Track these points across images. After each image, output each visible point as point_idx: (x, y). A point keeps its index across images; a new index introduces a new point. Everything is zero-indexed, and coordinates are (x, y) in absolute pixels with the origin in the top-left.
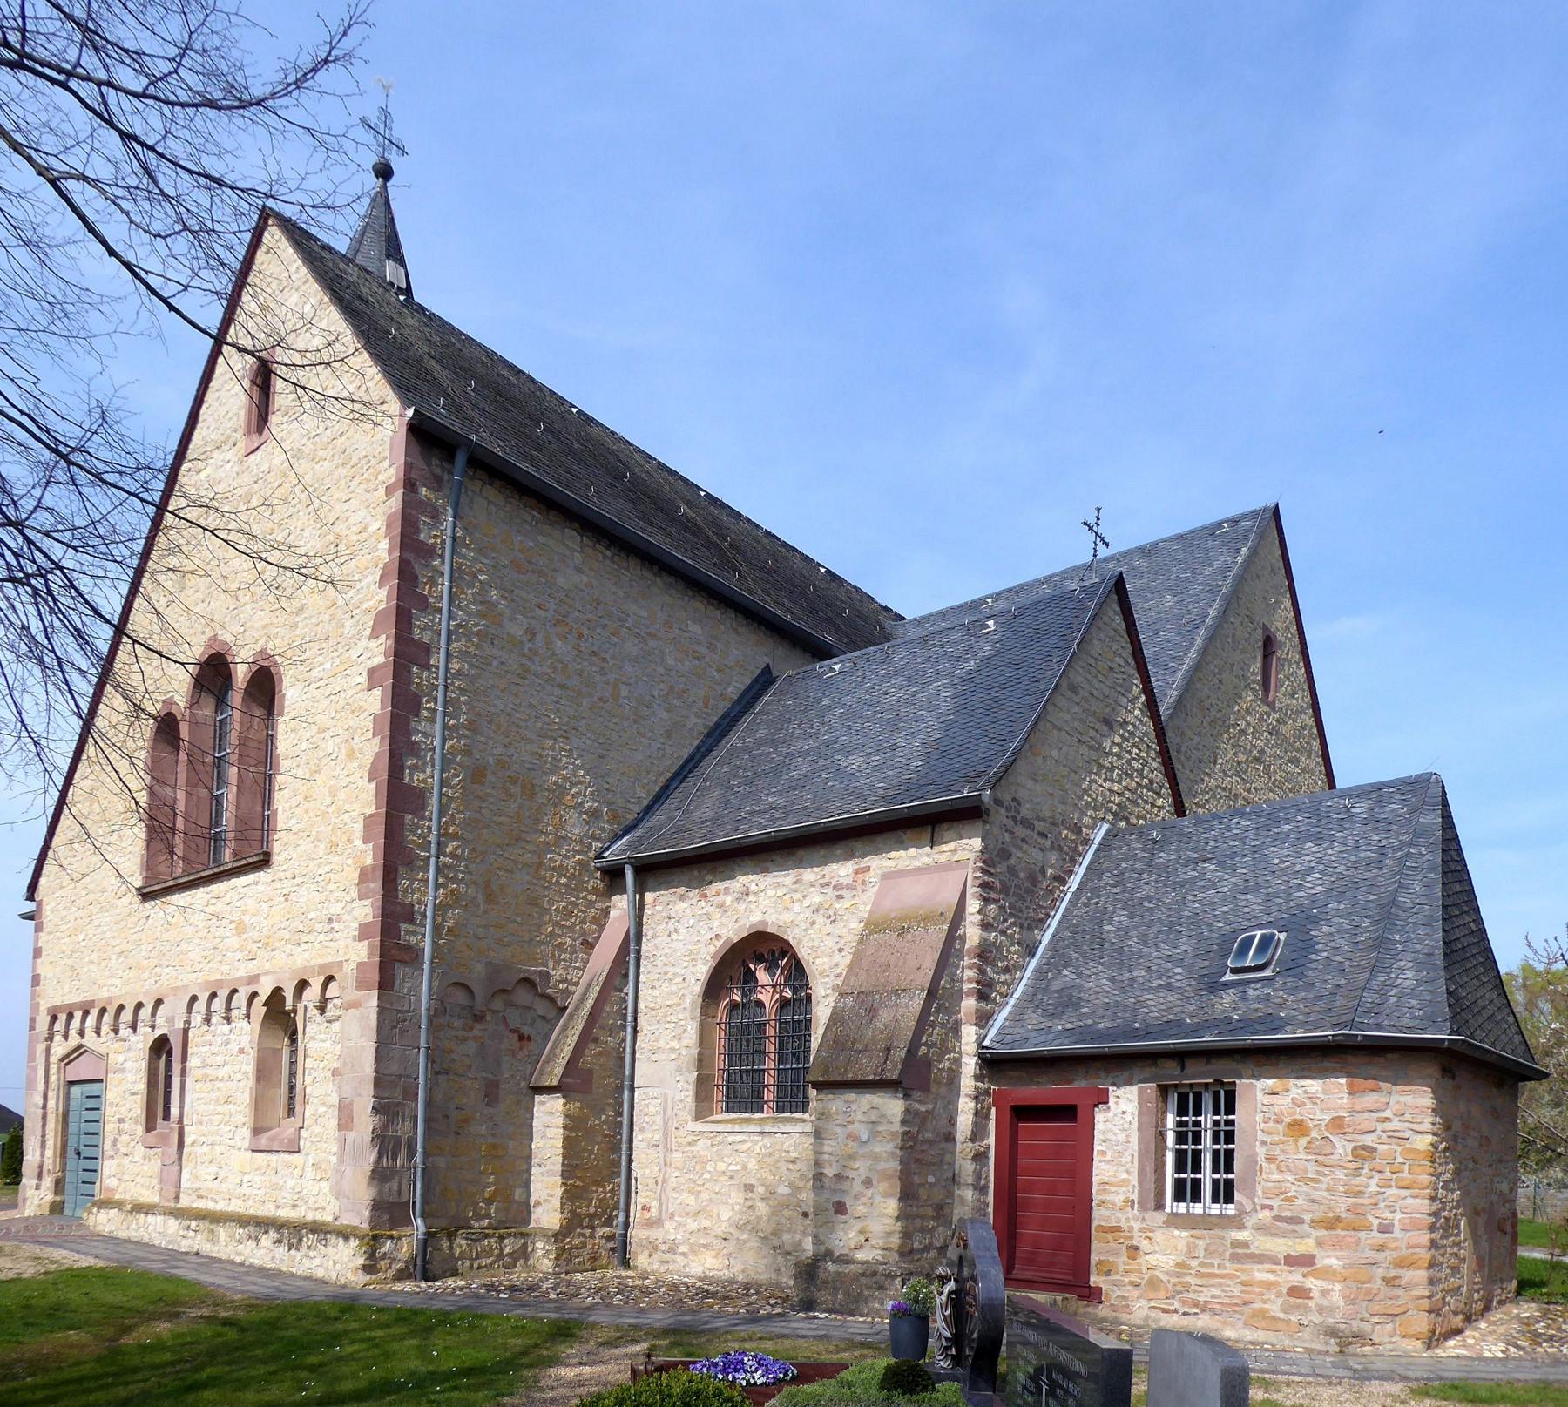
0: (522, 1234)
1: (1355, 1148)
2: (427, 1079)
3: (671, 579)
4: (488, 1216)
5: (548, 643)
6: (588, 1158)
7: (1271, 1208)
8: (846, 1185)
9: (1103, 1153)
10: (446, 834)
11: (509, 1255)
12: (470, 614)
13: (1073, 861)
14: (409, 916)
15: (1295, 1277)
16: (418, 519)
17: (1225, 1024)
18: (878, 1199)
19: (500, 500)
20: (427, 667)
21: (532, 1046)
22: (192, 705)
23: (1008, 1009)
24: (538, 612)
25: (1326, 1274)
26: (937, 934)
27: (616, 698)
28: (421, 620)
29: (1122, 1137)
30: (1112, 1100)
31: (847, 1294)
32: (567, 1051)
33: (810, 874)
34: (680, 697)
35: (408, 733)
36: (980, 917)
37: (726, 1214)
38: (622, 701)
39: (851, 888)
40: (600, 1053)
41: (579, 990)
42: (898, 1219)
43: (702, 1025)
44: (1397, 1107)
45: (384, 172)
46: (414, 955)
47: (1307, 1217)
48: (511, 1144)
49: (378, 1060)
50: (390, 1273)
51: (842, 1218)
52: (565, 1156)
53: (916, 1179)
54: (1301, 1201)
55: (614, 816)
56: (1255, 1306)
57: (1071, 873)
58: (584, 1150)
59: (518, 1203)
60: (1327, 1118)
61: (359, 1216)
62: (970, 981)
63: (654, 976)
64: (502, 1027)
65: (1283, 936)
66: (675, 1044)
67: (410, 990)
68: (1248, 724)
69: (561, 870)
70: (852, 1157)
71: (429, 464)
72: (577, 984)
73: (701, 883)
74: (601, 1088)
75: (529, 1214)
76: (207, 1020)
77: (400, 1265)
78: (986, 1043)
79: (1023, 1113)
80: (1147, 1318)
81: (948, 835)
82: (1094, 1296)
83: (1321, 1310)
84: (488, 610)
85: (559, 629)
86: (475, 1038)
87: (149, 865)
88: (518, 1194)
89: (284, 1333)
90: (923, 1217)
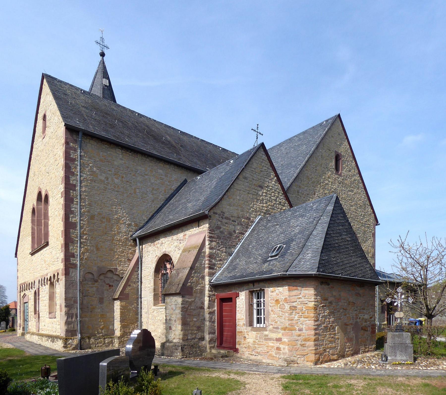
1: (290, 307)
2: (80, 298)
3: (152, 159)
4: (102, 333)
5: (113, 180)
6: (129, 317)
7: (272, 325)
8: (171, 322)
9: (238, 311)
10: (83, 234)
11: (107, 343)
12: (88, 175)
13: (247, 228)
14: (73, 256)
15: (277, 344)
16: (70, 152)
17: (263, 273)
18: (177, 325)
19: (95, 144)
20: (75, 190)
21: (113, 288)
22: (37, 205)
23: (221, 271)
24: (109, 172)
25: (284, 343)
26: (195, 252)
27: (135, 193)
28: (72, 178)
29: (242, 306)
30: (240, 296)
31: (170, 351)
33: (175, 237)
34: (156, 191)
35: (70, 208)
36: (209, 246)
37: (160, 331)
38: (137, 194)
39: (183, 240)
42: (182, 330)
43: (154, 280)
44: (303, 294)
45: (103, 55)
46: (75, 266)
47: (280, 327)
48: (108, 314)
49: (65, 294)
50: (71, 348)
51: (171, 331)
52: (121, 317)
53: (188, 320)
54: (278, 323)
55: (136, 225)
56: (270, 353)
57: (246, 231)
58: (127, 315)
60: (284, 298)
61: (63, 335)
62: (207, 264)
63: (145, 268)
65: (284, 246)
66: (149, 286)
67: (74, 275)
68: (329, 182)
69: (120, 241)
70: (172, 314)
71: (72, 137)
72: (126, 271)
73: (154, 242)
74: (131, 299)
75: (114, 332)
76: (42, 285)
77: (74, 346)
78: (212, 281)
79: (223, 300)
80: (247, 357)
81: (202, 224)
82: (236, 350)
83: (283, 353)
84: (93, 173)
85: (116, 176)
86: (96, 287)
87: (33, 247)
88: (111, 327)
89: (283, 375)
90: (192, 330)
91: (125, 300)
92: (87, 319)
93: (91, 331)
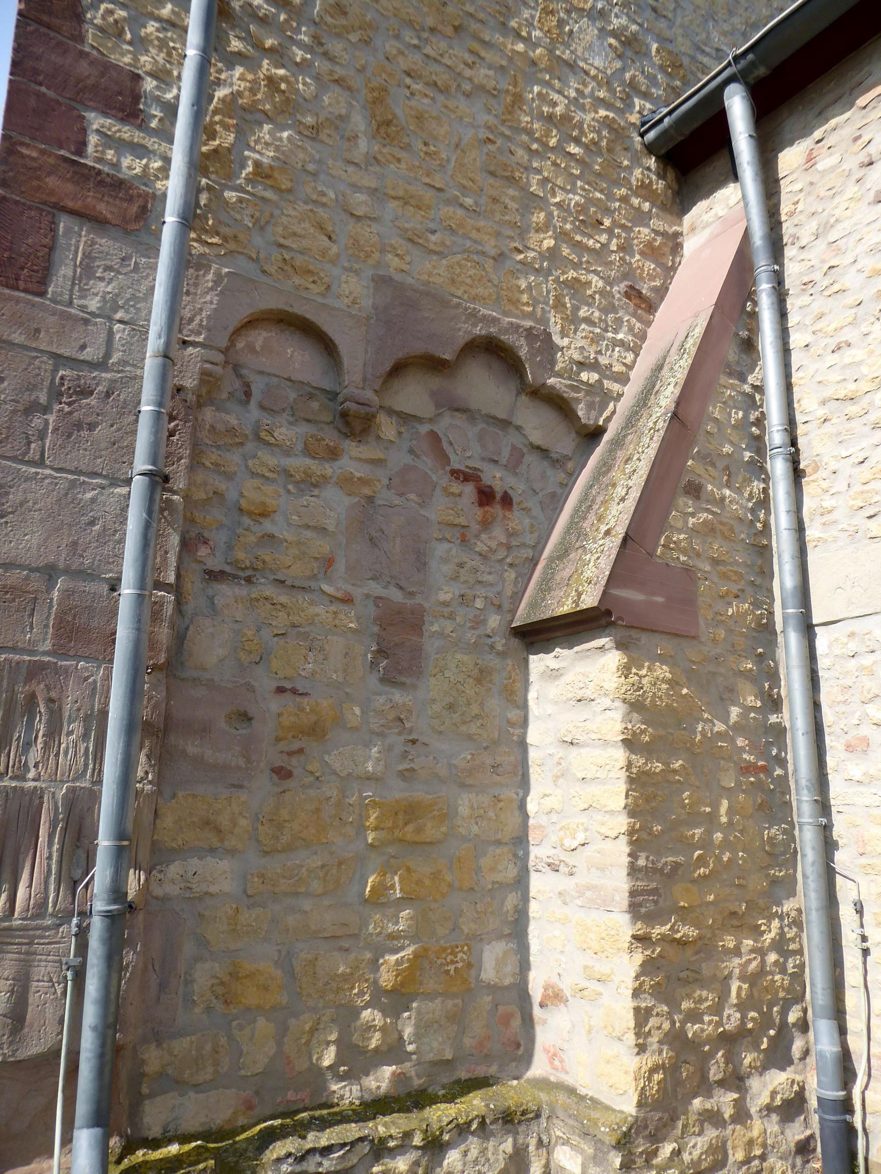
0: (510, 1119)
2: (149, 580)
4: (393, 1051)
6: (706, 843)
21: (517, 520)
32: (618, 515)
40: (709, 530)
41: (631, 391)
48: (465, 804)
52: (638, 841)
58: (693, 818)
59: (492, 988)
64: (427, 463)
67: (111, 305)
75: (528, 1022)
86: (346, 482)
91: (662, 646)
92: (219, 875)
93: (259, 1046)
